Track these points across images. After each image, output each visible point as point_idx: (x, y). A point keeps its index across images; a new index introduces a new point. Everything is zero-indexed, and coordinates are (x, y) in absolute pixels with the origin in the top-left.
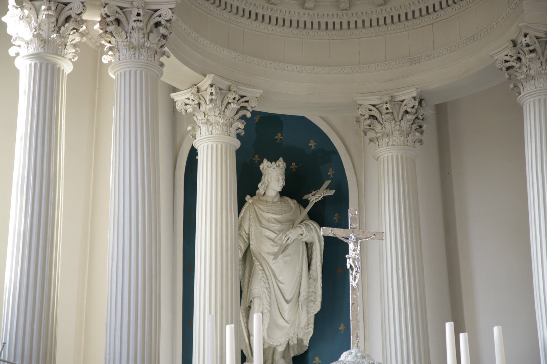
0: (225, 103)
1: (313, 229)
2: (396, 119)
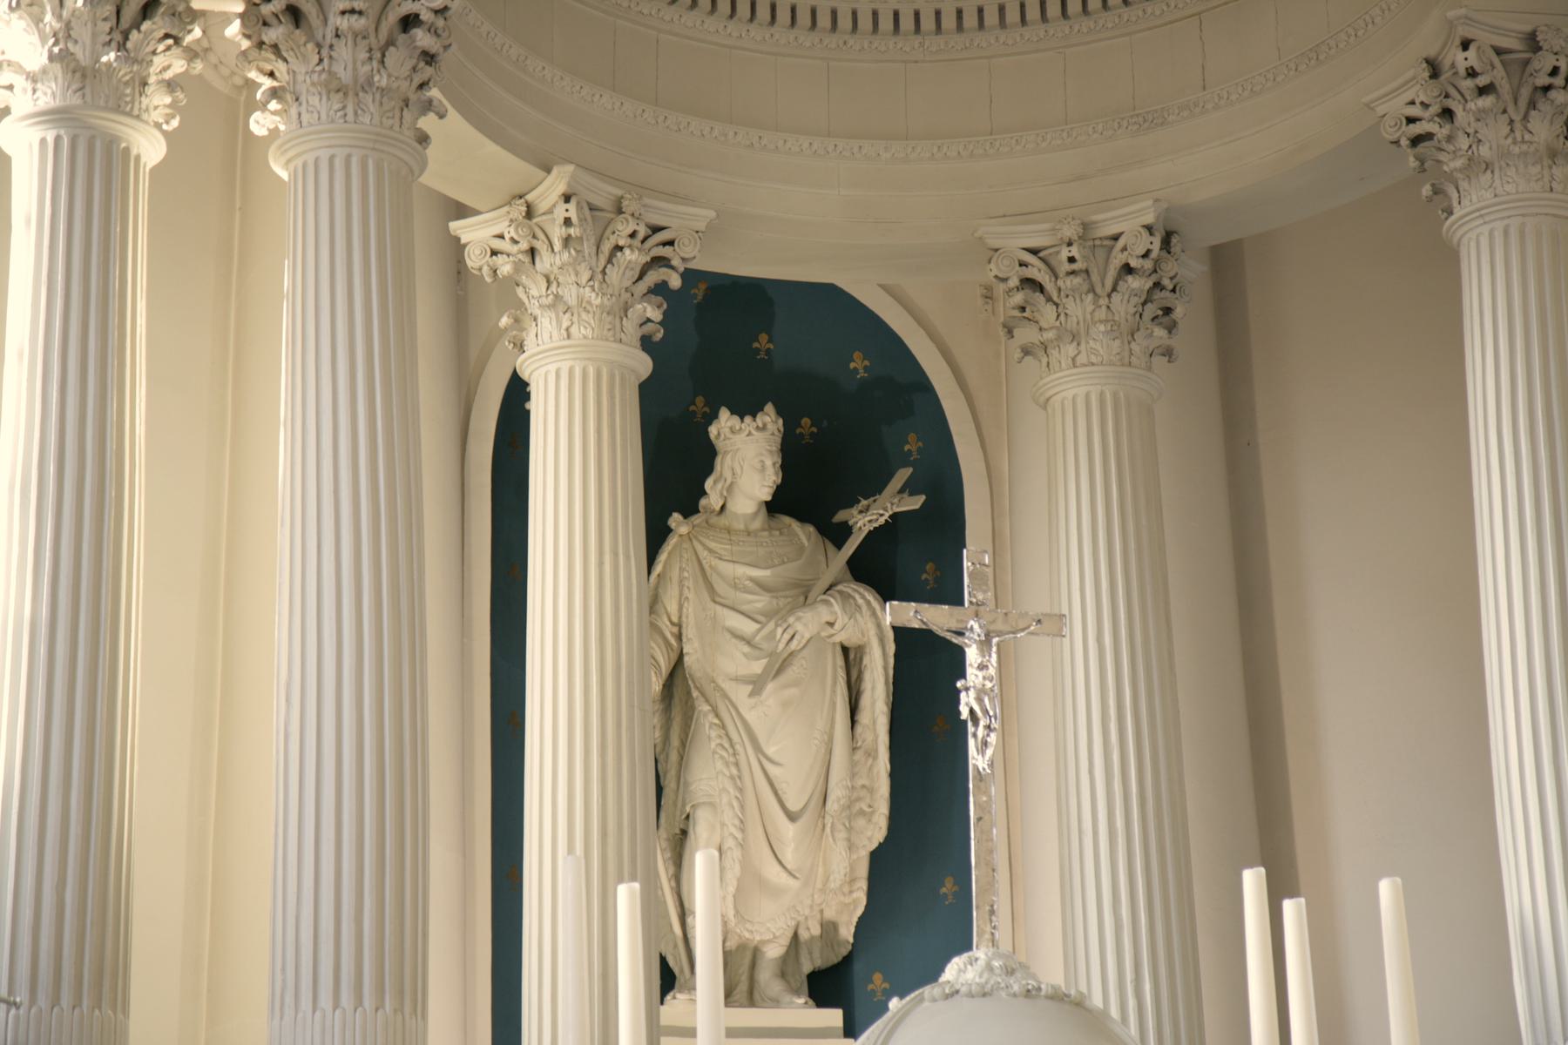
1: (864, 608)
2: (1099, 290)
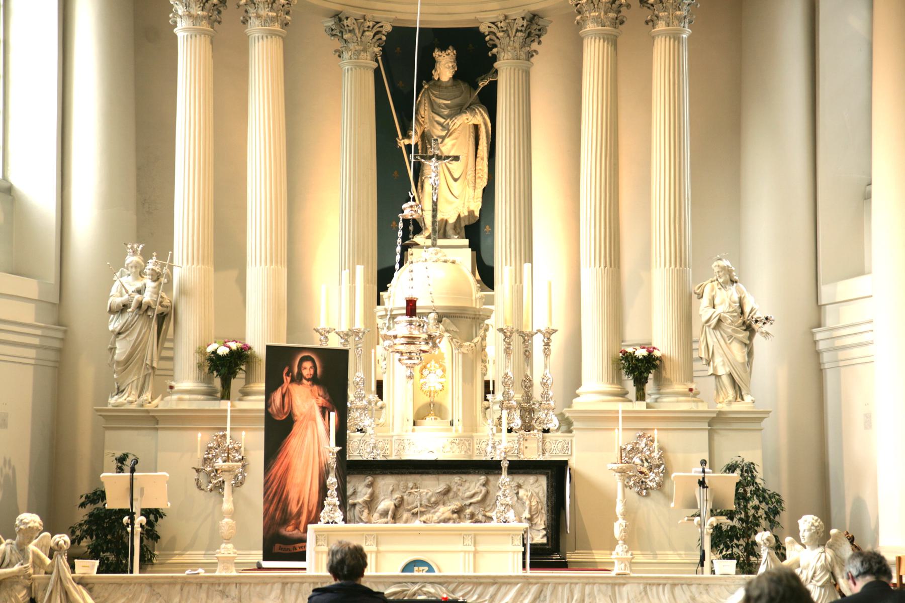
0: (361, 31)
1: (479, 113)
2: (511, 34)
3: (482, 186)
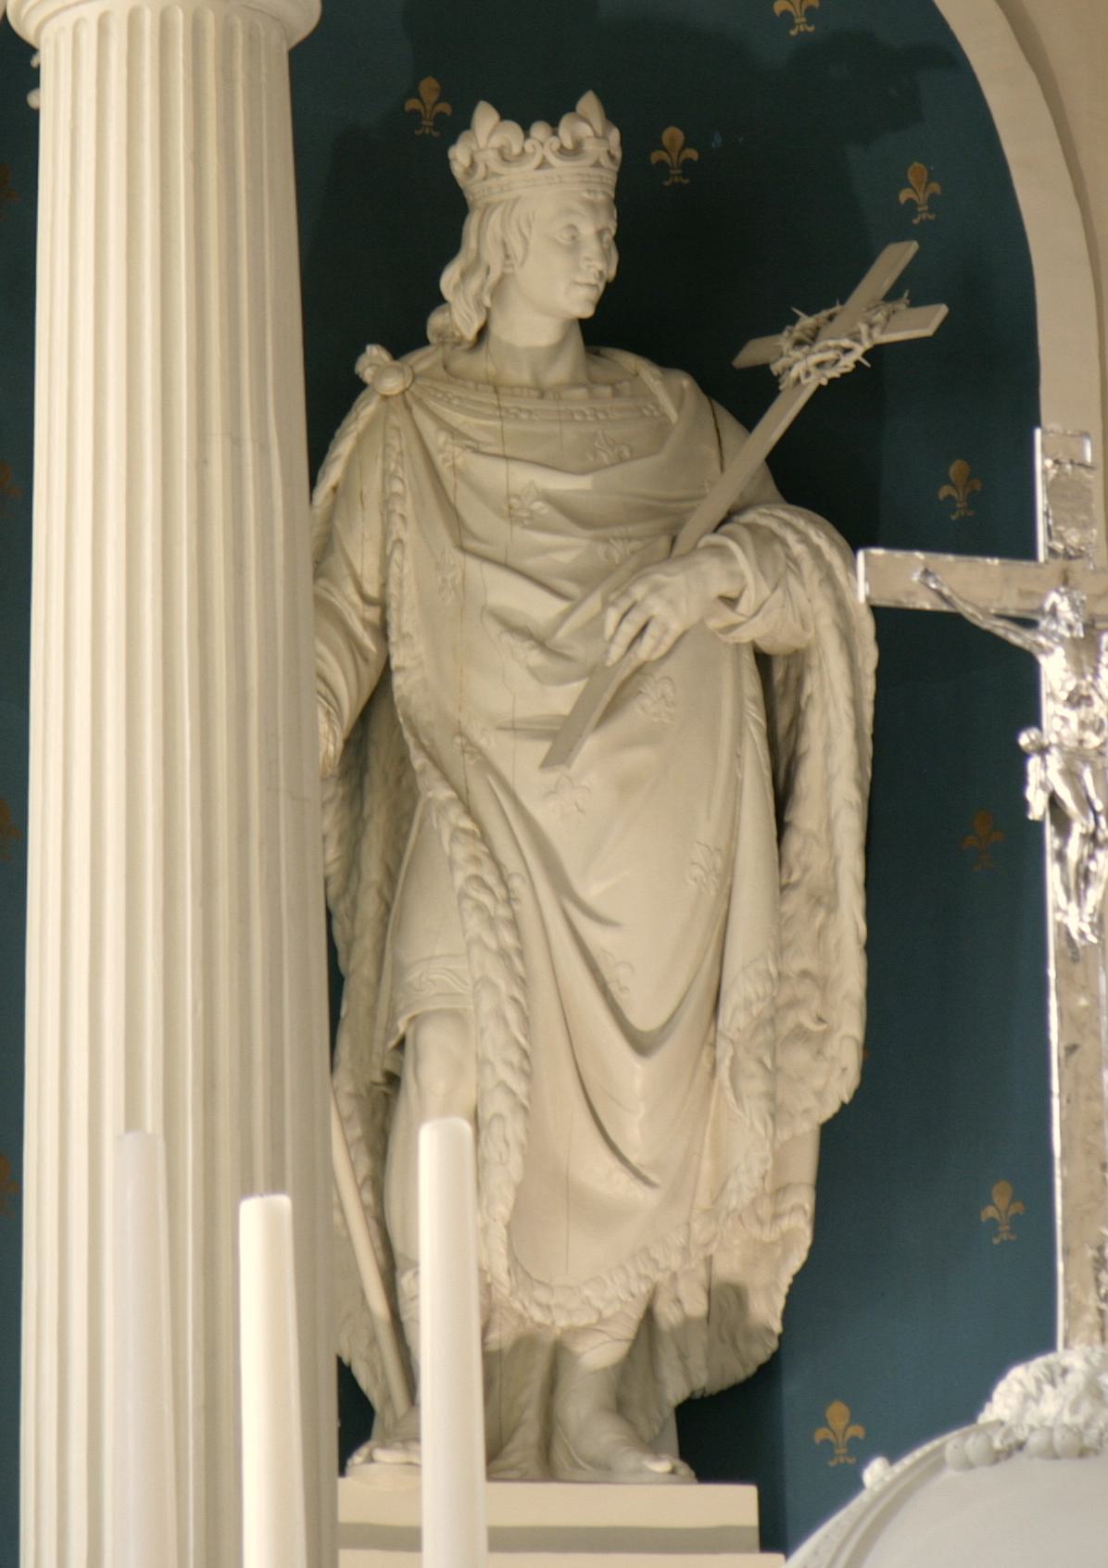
1: (807, 564)
3: (820, 1095)
